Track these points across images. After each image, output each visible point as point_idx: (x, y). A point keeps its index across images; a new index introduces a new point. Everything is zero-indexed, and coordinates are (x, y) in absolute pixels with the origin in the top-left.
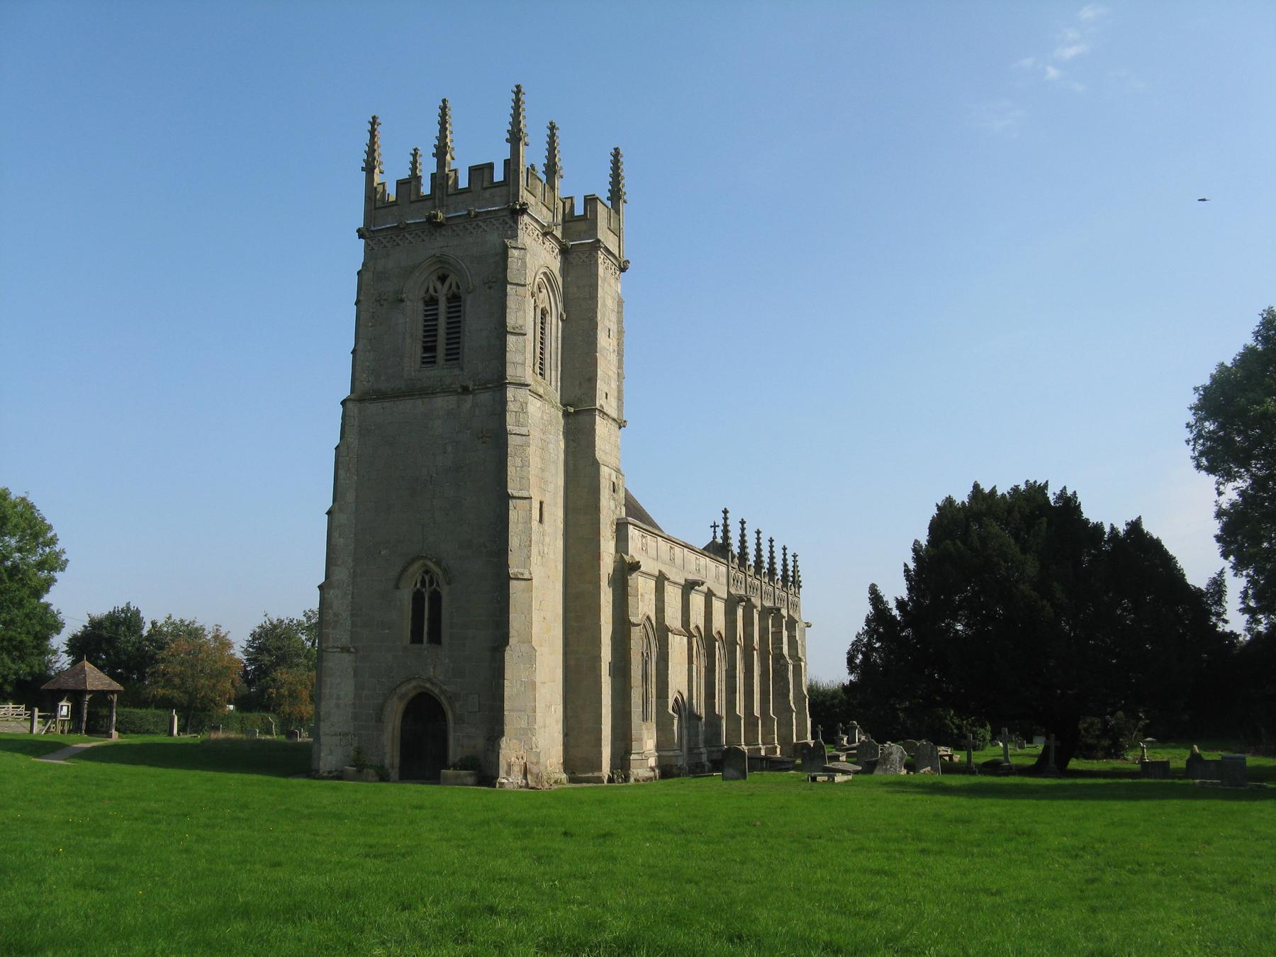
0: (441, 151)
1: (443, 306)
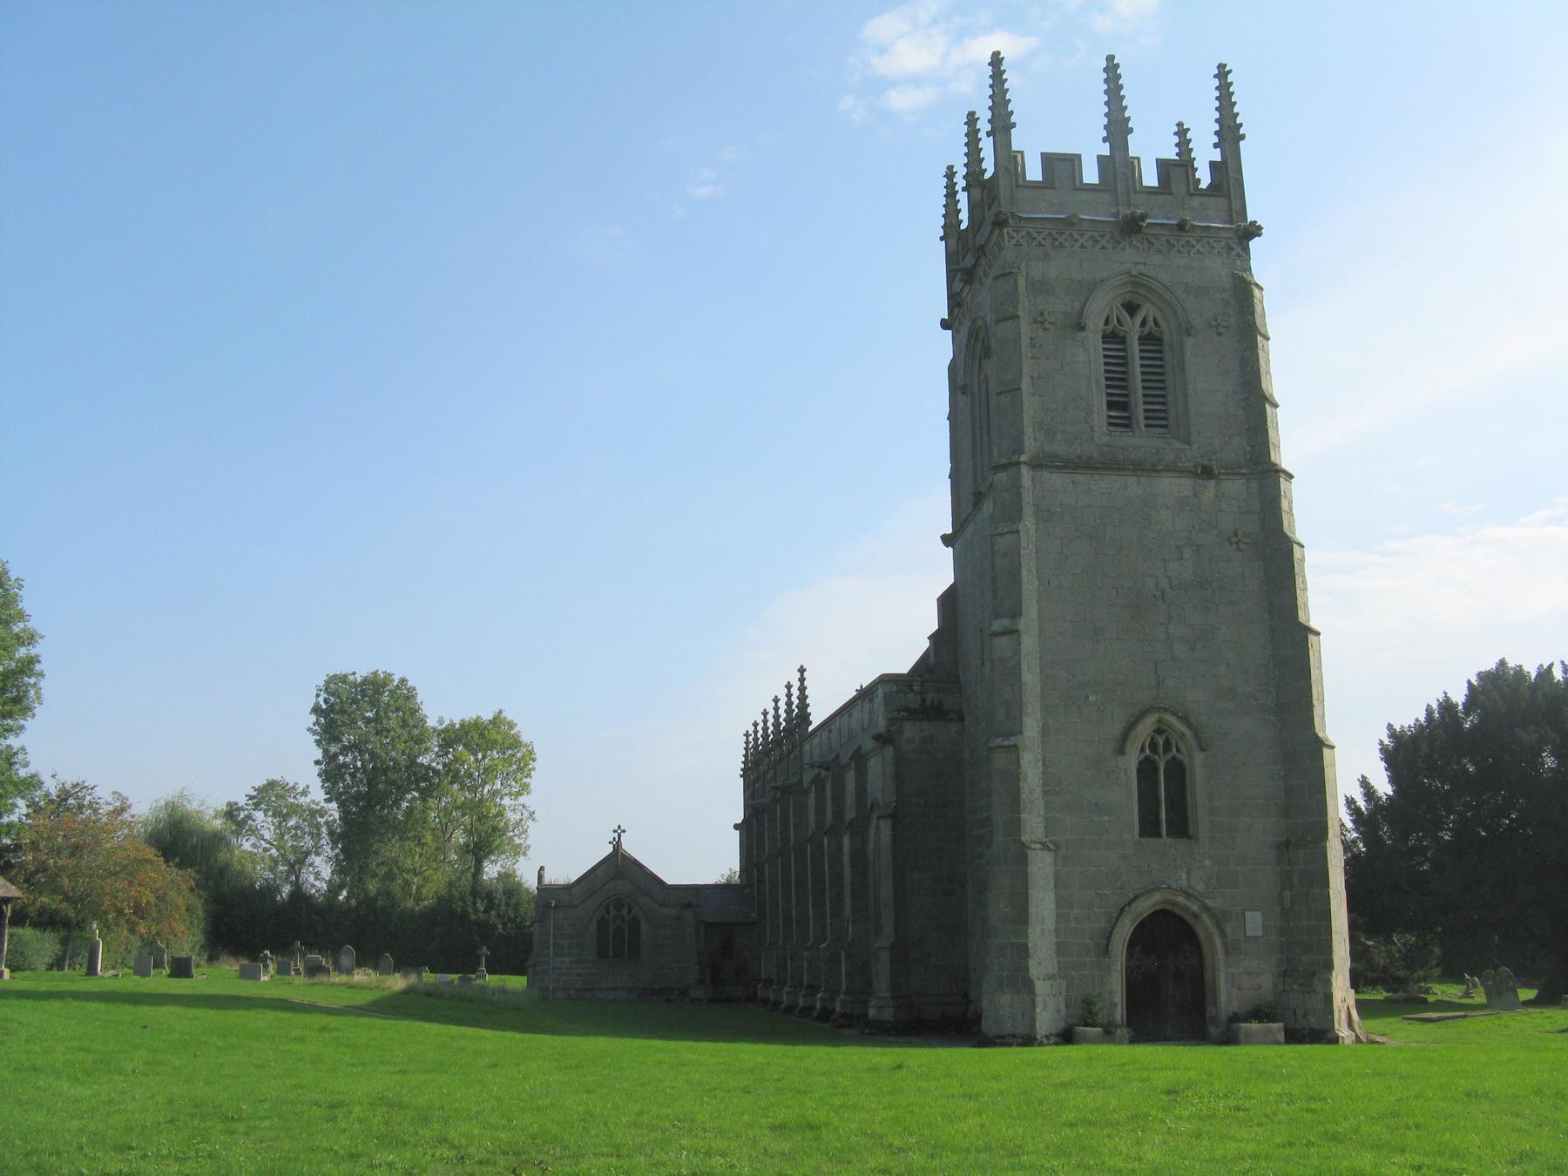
0: (1117, 128)
1: (1135, 348)
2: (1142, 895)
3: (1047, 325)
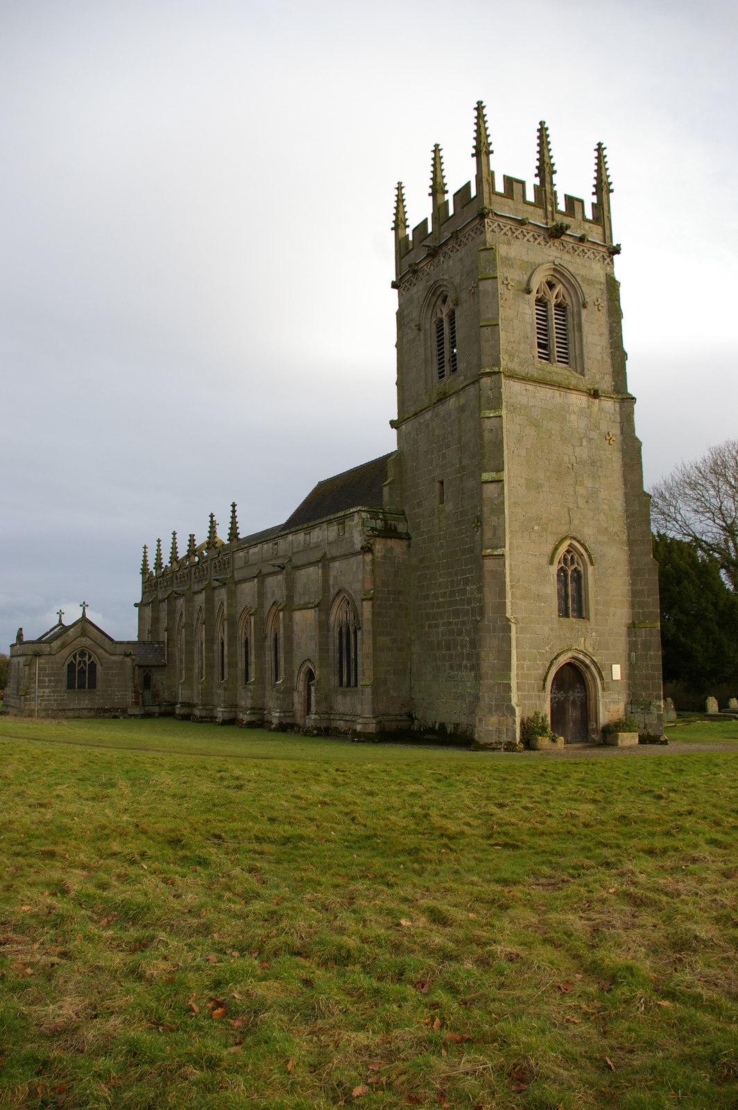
2: (562, 653)
3: (509, 287)
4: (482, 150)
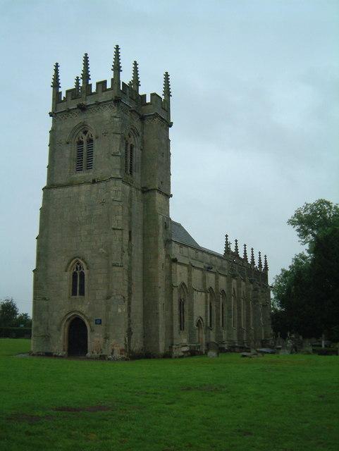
1: (85, 146)
4: (117, 68)
